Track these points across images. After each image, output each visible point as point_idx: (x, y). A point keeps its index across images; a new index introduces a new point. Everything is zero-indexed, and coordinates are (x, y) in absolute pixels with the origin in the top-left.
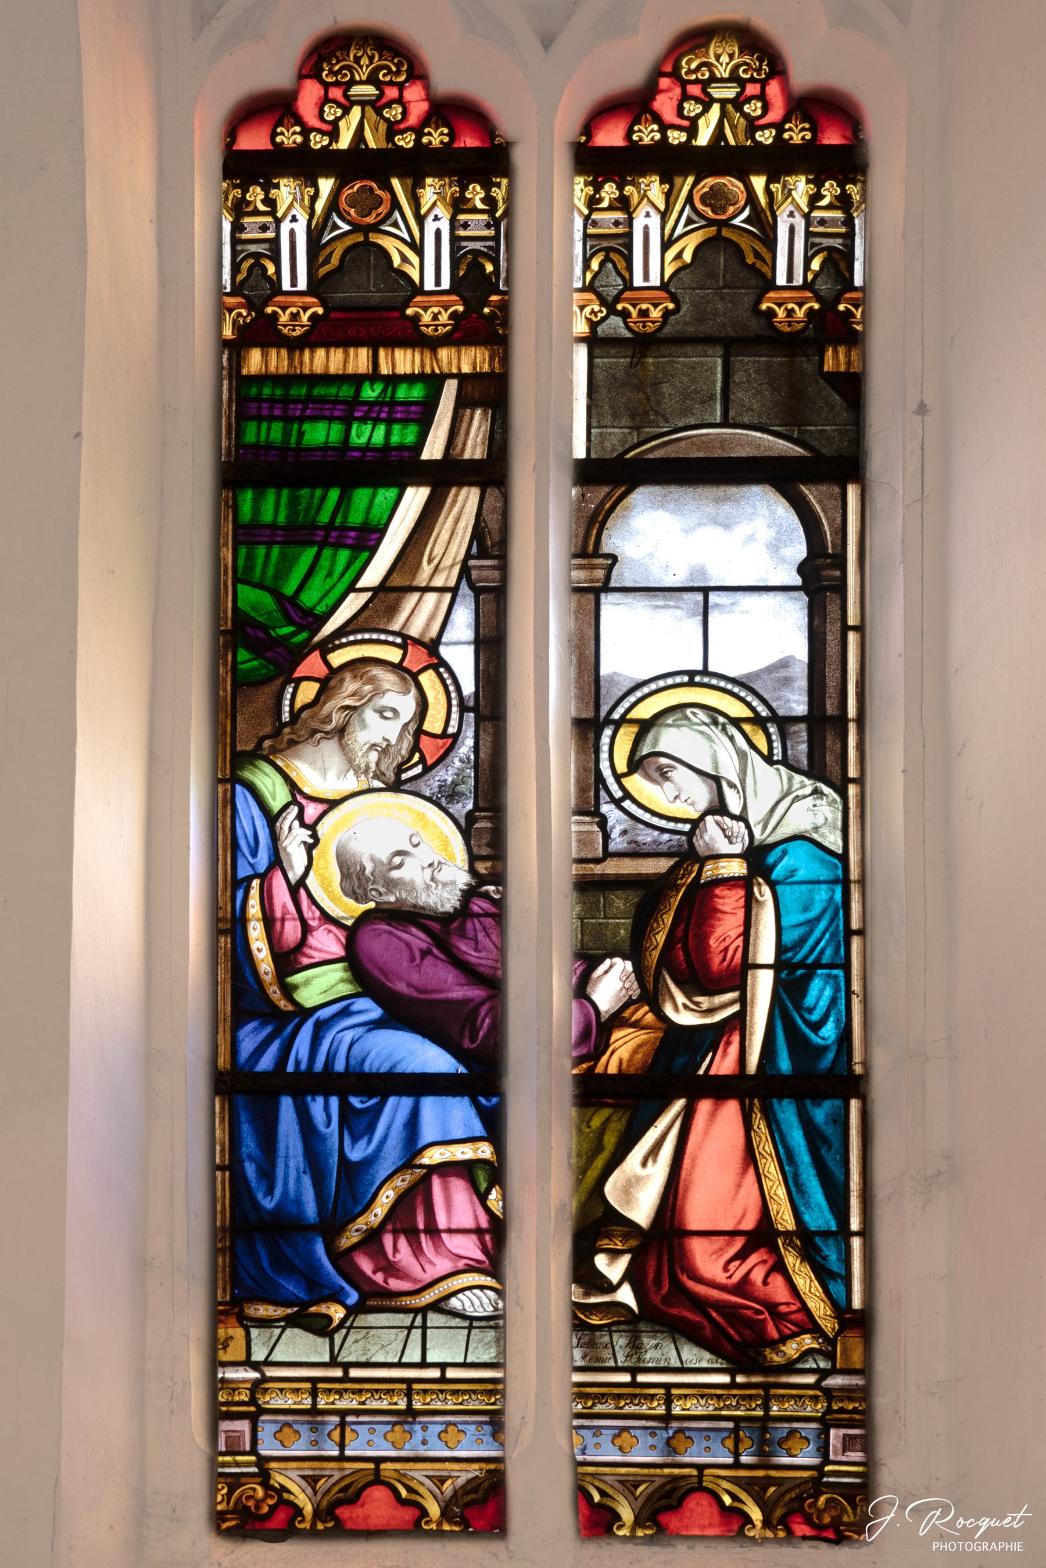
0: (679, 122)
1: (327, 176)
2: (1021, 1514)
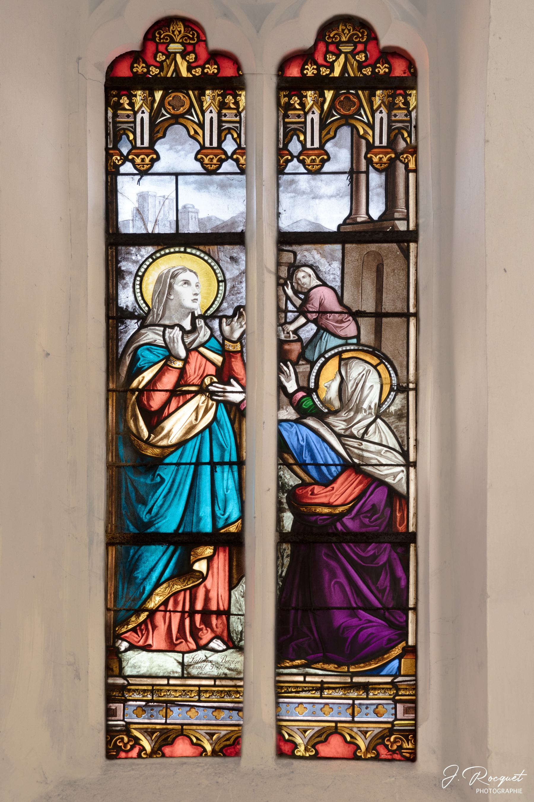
0: (325, 63)
1: (329, 90)
2: (521, 774)
